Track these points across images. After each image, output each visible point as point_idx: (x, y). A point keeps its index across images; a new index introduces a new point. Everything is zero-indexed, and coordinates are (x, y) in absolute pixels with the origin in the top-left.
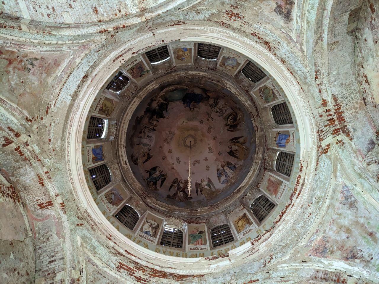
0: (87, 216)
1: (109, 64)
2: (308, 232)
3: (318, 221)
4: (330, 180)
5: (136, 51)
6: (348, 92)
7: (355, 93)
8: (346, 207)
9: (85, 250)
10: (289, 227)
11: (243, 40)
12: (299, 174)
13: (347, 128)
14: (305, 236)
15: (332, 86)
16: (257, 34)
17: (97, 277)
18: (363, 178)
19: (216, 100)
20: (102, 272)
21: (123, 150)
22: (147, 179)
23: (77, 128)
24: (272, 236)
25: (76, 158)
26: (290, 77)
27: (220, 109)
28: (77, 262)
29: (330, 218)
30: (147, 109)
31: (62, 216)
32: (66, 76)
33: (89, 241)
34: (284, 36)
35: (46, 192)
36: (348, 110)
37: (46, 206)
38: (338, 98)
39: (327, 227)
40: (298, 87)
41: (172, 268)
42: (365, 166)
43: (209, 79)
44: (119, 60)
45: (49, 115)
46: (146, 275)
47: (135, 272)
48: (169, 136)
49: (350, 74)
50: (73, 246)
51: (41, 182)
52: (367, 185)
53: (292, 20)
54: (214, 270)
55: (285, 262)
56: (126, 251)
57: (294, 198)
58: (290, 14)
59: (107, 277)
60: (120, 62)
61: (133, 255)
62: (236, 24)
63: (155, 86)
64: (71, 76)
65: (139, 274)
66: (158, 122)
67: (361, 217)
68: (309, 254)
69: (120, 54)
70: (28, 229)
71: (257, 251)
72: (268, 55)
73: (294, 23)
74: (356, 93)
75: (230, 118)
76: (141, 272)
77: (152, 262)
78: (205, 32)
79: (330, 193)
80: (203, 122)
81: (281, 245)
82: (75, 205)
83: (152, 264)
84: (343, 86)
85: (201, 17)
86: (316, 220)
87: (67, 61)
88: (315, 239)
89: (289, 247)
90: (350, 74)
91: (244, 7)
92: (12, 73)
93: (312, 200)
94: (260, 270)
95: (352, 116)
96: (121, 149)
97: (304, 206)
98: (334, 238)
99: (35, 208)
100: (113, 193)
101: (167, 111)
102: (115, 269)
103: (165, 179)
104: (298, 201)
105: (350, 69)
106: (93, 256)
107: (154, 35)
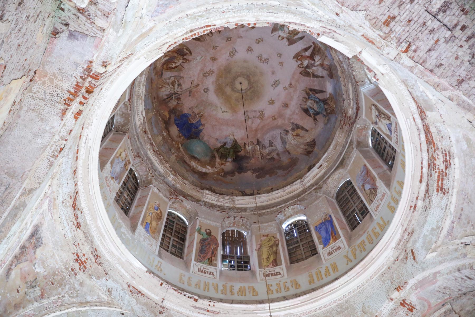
0: (401, 244)
5: (192, 300)
6: (43, 105)
7: (36, 95)
9: (439, 243)
11: (92, 222)
13: (83, 75)
15: (55, 130)
16: (76, 224)
19: (167, 100)
20: (457, 213)
21: (306, 180)
22: (326, 117)
23: (310, 303)
26: (83, 149)
27: (174, 86)
28: (457, 253)
30: (240, 173)
31: (412, 285)
34: (53, 209)
36: (62, 89)
37: (408, 305)
38: (60, 111)
40: (85, 133)
41: (414, 118)
43: (151, 144)
44: (213, 309)
46: (438, 155)
47: (441, 170)
48: (254, 117)
49: (23, 120)
54: (386, 68)
56: (421, 181)
58: (32, 234)
59: (461, 206)
60: (214, 306)
61: (422, 172)
62: (86, 250)
63: (208, 194)
65: (440, 163)
66: (245, 144)
69: (208, 313)
71: (324, 27)
72: (83, 187)
73: (35, 222)
74: (35, 93)
75: (174, 65)
76: (437, 162)
77: (419, 145)
78: (119, 259)
80: (205, 89)
82: (395, 266)
83: (421, 144)
84: (42, 116)
85: (110, 284)
90: (23, 120)
91: (66, 266)
95: (64, 78)
96: (306, 183)
99: (417, 312)
100: (363, 186)
101: (225, 144)
102: (447, 197)
103: (311, 90)
105: (18, 125)
106: (443, 231)
107: (164, 299)
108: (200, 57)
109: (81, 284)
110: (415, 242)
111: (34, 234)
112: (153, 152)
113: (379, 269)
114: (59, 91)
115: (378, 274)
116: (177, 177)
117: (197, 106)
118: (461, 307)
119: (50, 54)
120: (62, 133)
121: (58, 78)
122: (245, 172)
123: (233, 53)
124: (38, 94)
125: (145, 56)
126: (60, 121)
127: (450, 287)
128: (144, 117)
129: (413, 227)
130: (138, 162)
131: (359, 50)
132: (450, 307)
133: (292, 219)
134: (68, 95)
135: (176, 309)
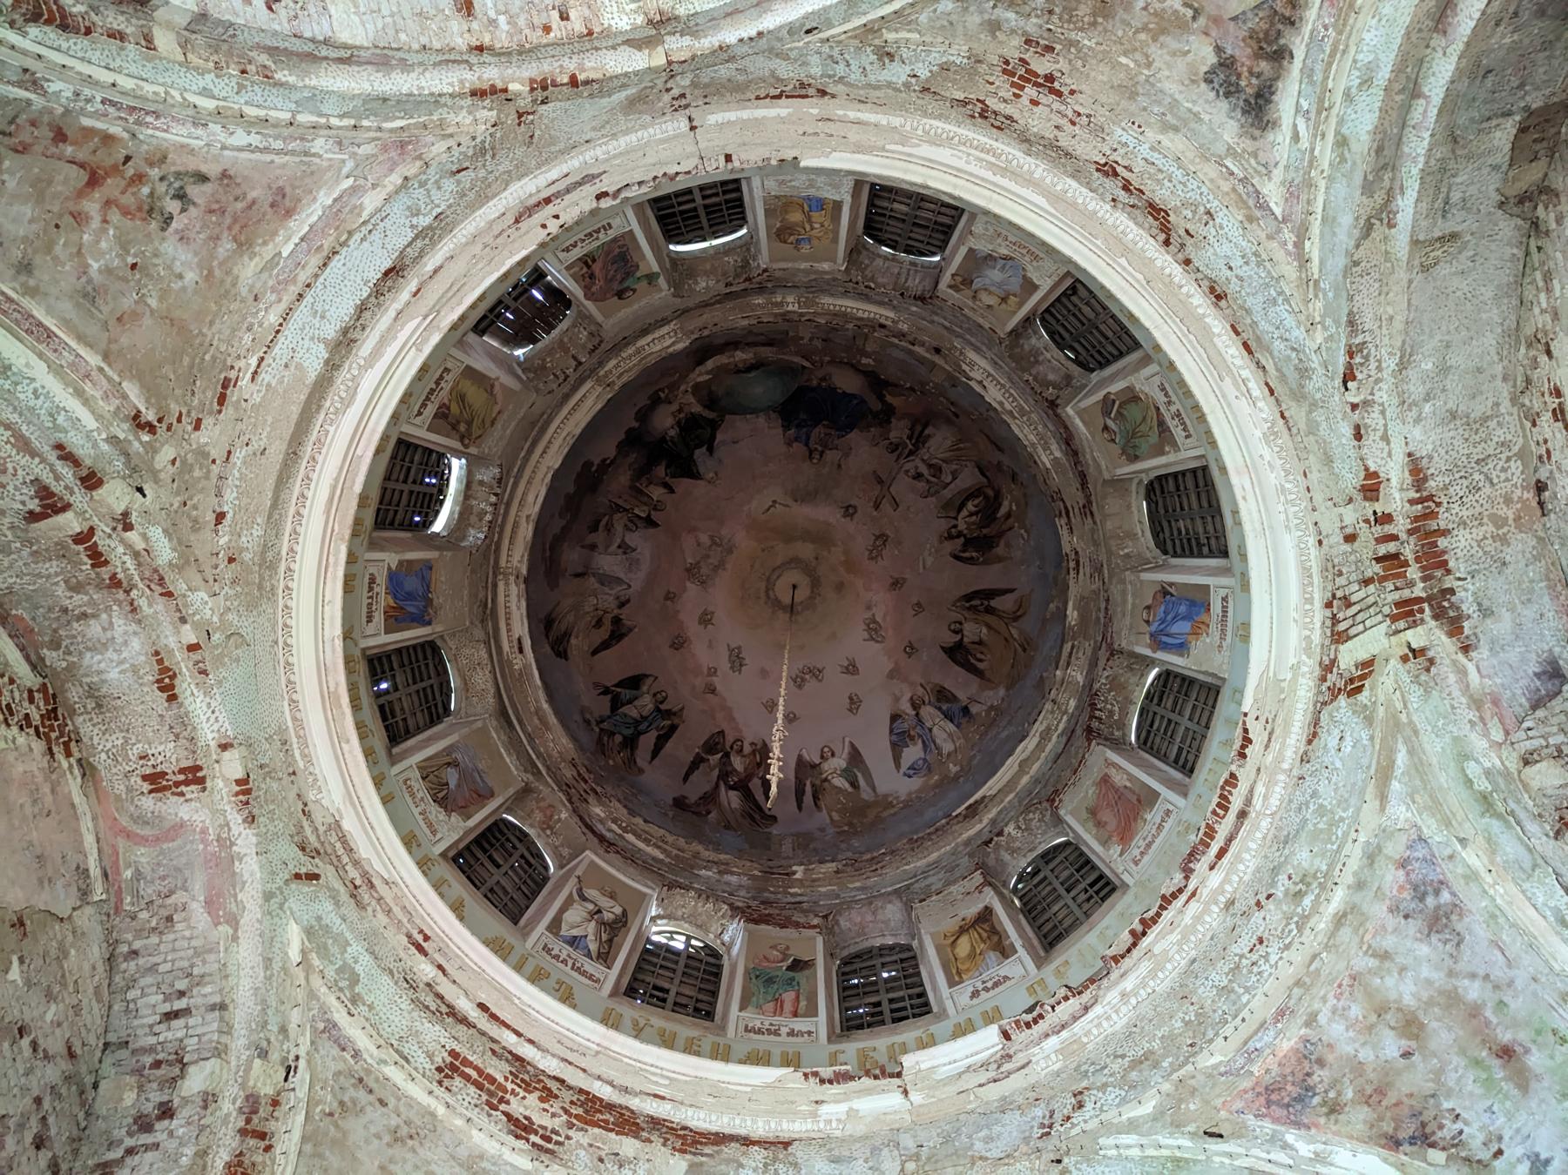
0: (338, 845)
1: (497, 229)
2: (1245, 1013)
3: (1288, 973)
4: (1358, 810)
5: (611, 190)
7: (1503, 456)
8: (1412, 927)
9: (316, 982)
10: (1165, 981)
11: (1059, 188)
12: (1233, 768)
13: (1453, 599)
14: (1228, 1030)
16: (1119, 169)
17: (354, 1101)
18: (1499, 816)
19: (919, 428)
20: (377, 1080)
21: (514, 590)
23: (337, 480)
24: (1091, 1015)
25: (320, 602)
26: (1238, 362)
27: (930, 466)
28: (275, 1029)
29: (1342, 965)
30: (630, 431)
32: (315, 261)
33: (335, 950)
34: (1234, 190)
35: (182, 729)
37: (177, 784)
39: (1324, 1000)
40: (1266, 409)
41: (663, 1098)
42: (1513, 764)
44: (538, 218)
45: (229, 411)
46: (554, 1115)
49: (1494, 377)
50: (268, 962)
51: (167, 686)
52: (1510, 847)
53: (1274, 124)
54: (834, 1125)
55: (1132, 1126)
56: (482, 1007)
57: (1201, 866)
59: (392, 1102)
60: (544, 226)
61: (508, 1027)
62: (1039, 118)
63: (673, 344)
64: (336, 263)
65: (526, 1105)
66: (672, 491)
67: (1473, 976)
68: (1239, 1105)
70: (95, 871)
71: (1023, 1067)
72: (1159, 263)
74: (1508, 459)
75: (970, 506)
76: (533, 1099)
79: (1354, 864)
81: (1123, 1056)
82: (292, 795)
85: (897, 73)
86: (1282, 967)
87: (325, 198)
88: (1268, 1046)
89: (1156, 1065)
90: (1494, 377)
92: (96, 223)
93: (1273, 884)
94: (1024, 1148)
96: (507, 584)
97: (1239, 907)
98: (1349, 1049)
99: (129, 789)
101: (711, 450)
103: (673, 728)
104: (1215, 879)
105: (1496, 358)
106: (344, 1013)
107: (693, 128)
108: (929, 563)
109: (994, 27)
110: (335, 897)
111: (1261, 102)
112: (882, 321)
113: (304, 742)
114: (1465, 513)
115: (292, 730)
116: (776, 315)
117: (839, 466)
118: (83, 934)
119: (1548, 579)
120: (1376, 415)
121: (1490, 541)
122: (620, 446)
123: (873, 631)
124: (1501, 463)
125: (1284, 685)
126: (1411, 448)
127: (164, 938)
128: (970, 379)
129: (370, 909)
130: (909, 283)
131: (916, 1097)
132: (96, 898)
133: (457, 491)
134: (1442, 522)
135: (639, 134)
